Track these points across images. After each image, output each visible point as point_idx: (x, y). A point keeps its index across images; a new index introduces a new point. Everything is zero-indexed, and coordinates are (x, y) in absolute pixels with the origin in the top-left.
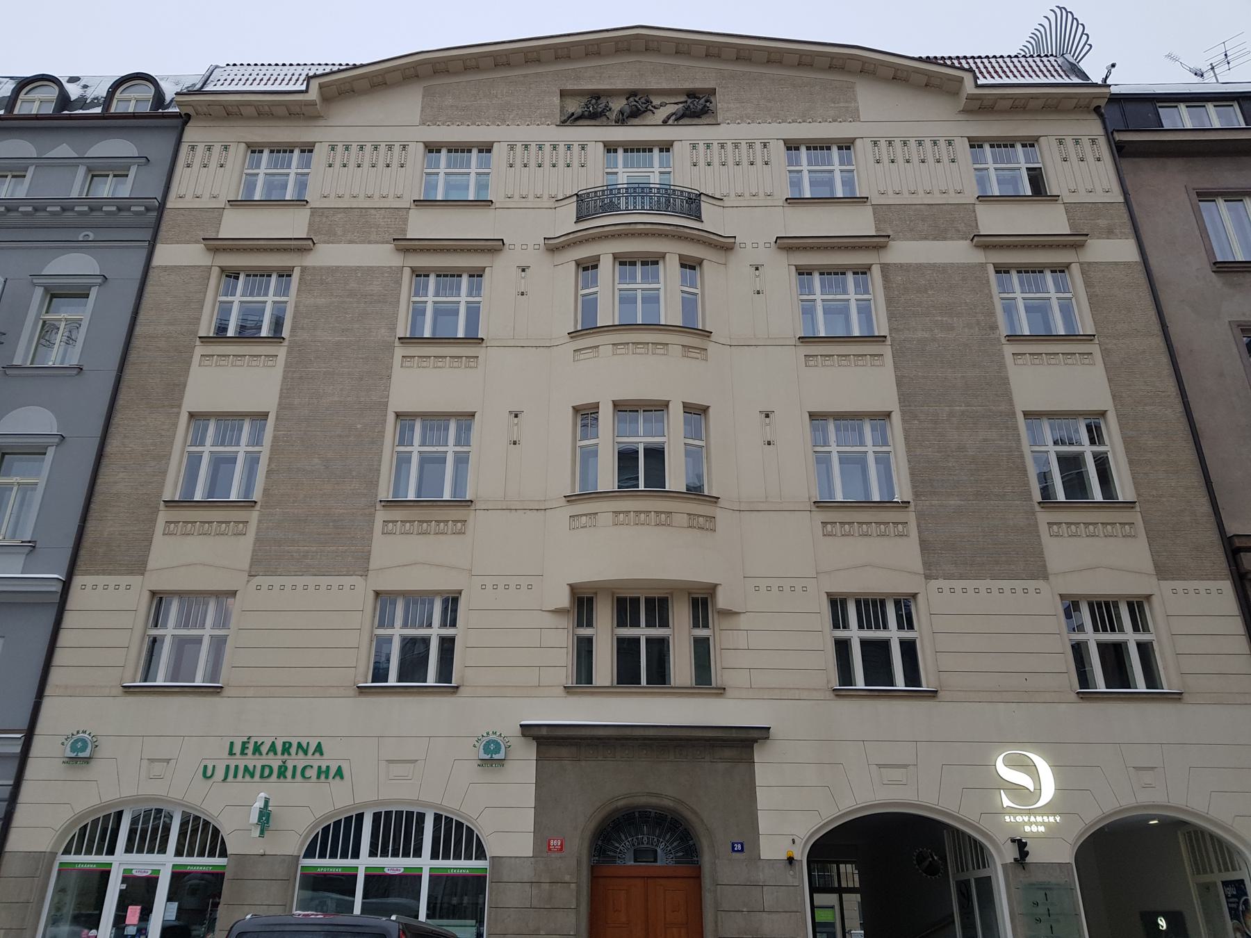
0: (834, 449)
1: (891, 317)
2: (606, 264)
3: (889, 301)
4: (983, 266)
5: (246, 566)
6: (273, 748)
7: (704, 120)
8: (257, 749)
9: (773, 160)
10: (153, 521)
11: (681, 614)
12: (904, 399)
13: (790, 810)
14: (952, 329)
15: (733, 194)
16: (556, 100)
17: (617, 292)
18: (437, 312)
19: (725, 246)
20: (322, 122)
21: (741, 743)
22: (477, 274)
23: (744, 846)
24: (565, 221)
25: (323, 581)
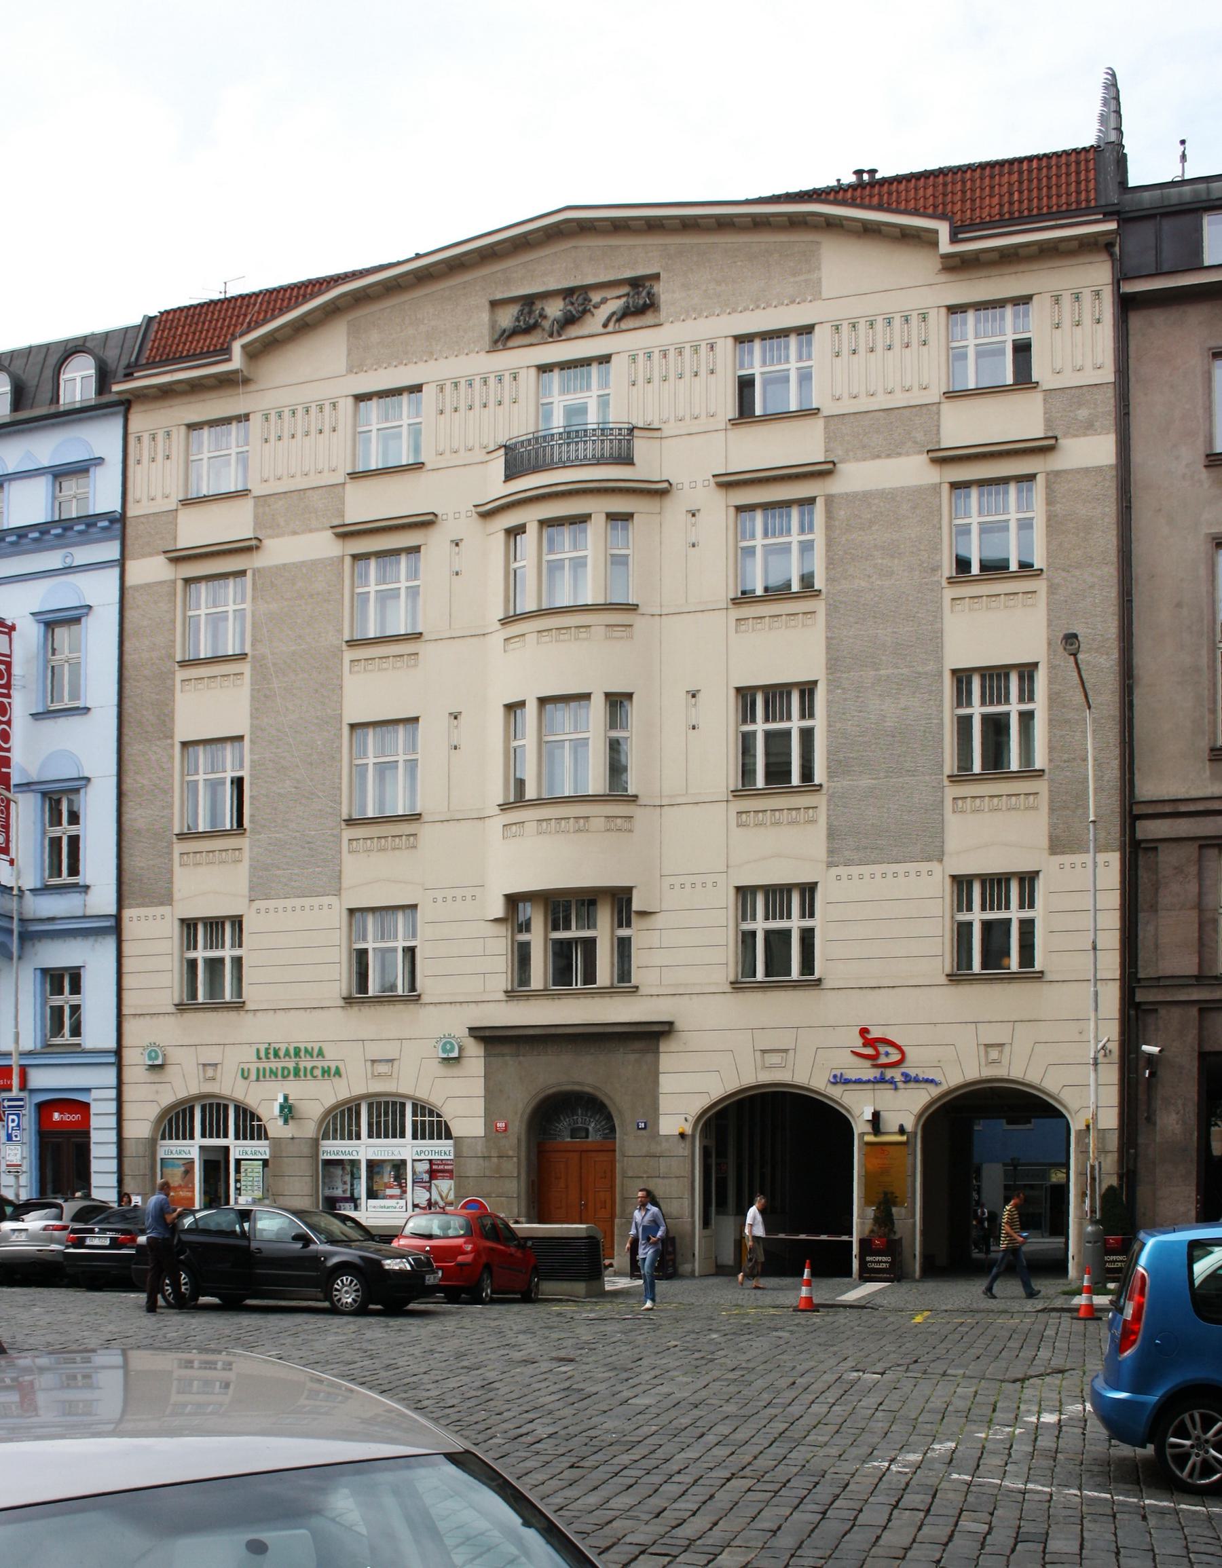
0: (975, 520)
2: (532, 529)
3: (830, 543)
4: (936, 488)
5: (246, 891)
6: (287, 1054)
7: (649, 318)
8: (276, 1055)
9: (720, 369)
10: (171, 853)
11: (604, 917)
12: (833, 664)
13: (686, 1090)
14: (891, 574)
16: (485, 316)
18: (985, 529)
19: (659, 492)
20: (252, 387)
21: (651, 1036)
22: (417, 549)
23: (649, 1126)
24: (493, 483)
25: (307, 902)
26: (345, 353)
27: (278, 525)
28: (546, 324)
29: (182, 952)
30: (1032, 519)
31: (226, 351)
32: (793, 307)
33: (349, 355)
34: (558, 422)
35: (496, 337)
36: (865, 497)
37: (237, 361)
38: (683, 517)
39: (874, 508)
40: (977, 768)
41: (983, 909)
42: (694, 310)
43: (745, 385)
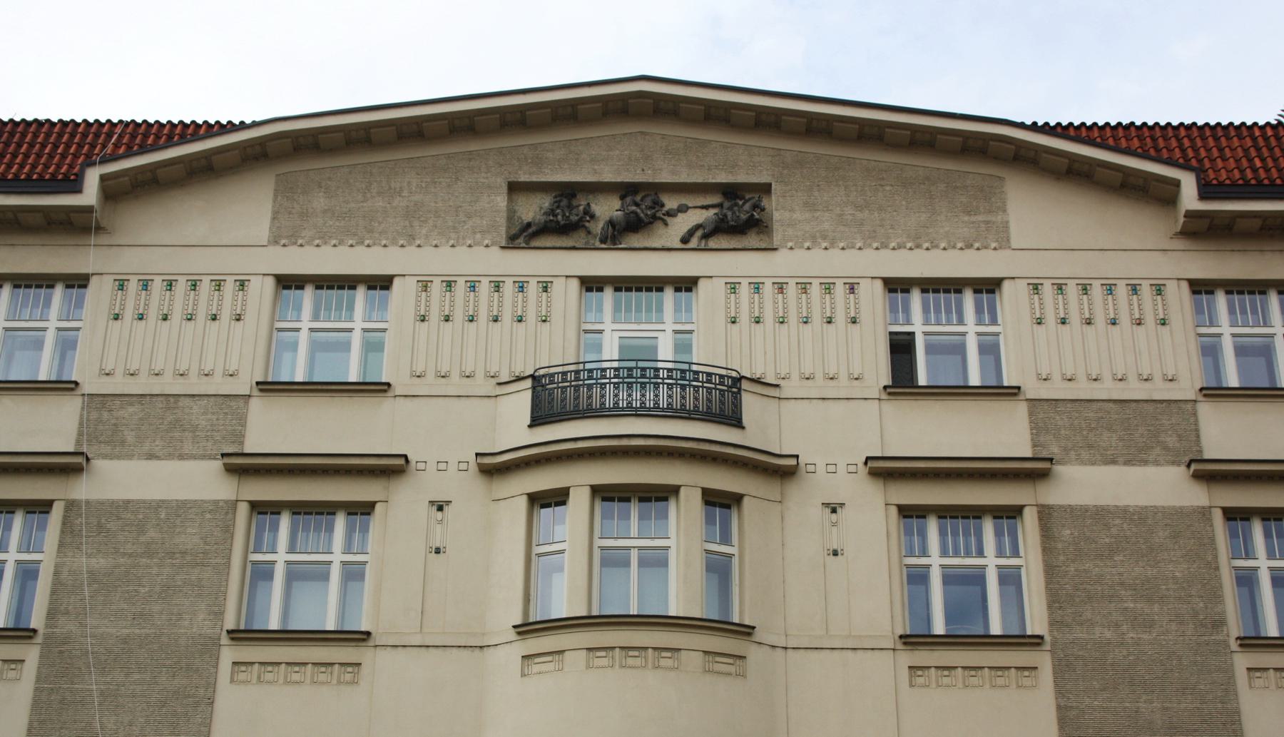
0: (935, 561)
1: (1054, 600)
2: (580, 500)
3: (1050, 571)
4: (1205, 513)
7: (752, 240)
9: (865, 317)
15: (795, 376)
16: (501, 201)
17: (597, 554)
19: (780, 471)
22: (366, 509)
24: (512, 425)
26: (269, 215)
27: (123, 442)
30: (39, 562)
31: (74, 185)
32: (970, 253)
33: (274, 219)
34: (610, 351)
35: (513, 231)
36: (1100, 515)
37: (90, 194)
38: (817, 514)
39: (1114, 531)
42: (824, 238)
43: (901, 348)
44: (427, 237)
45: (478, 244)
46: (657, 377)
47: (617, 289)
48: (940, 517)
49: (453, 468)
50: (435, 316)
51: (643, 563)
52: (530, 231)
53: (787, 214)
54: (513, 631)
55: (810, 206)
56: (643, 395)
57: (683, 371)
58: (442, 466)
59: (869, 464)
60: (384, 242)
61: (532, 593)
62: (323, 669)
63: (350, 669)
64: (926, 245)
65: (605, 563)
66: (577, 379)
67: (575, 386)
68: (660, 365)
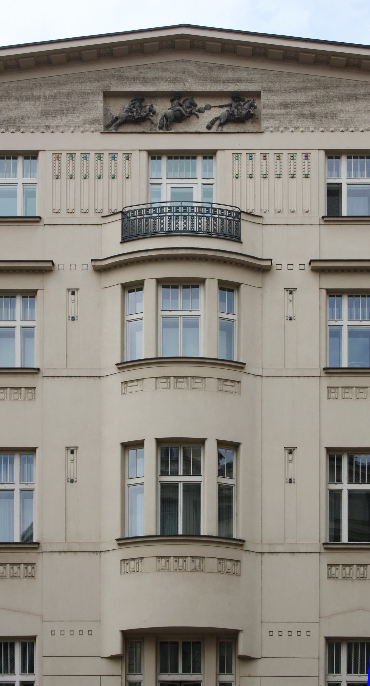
0: (345, 323)
2: (150, 287)
7: (249, 126)
9: (313, 174)
11: (210, 662)
15: (272, 211)
16: (100, 104)
17: (160, 319)
19: (261, 269)
22: (30, 294)
24: (110, 242)
28: (157, 120)
29: (326, 676)
34: (166, 196)
35: (108, 122)
40: (345, 537)
41: (349, 671)
42: (292, 125)
43: (333, 193)
44: (57, 126)
45: (87, 131)
46: (193, 212)
47: (170, 158)
48: (349, 296)
49: (79, 268)
50: (64, 175)
51: (185, 326)
52: (118, 122)
53: (270, 110)
54: (116, 367)
55: (284, 105)
56: (185, 223)
57: (208, 208)
58: (73, 267)
59: (312, 264)
60: (32, 130)
61: (125, 344)
62: (16, 391)
63: (30, 391)
64: (351, 129)
65: (164, 326)
66: (147, 214)
67: (146, 218)
68: (195, 204)
